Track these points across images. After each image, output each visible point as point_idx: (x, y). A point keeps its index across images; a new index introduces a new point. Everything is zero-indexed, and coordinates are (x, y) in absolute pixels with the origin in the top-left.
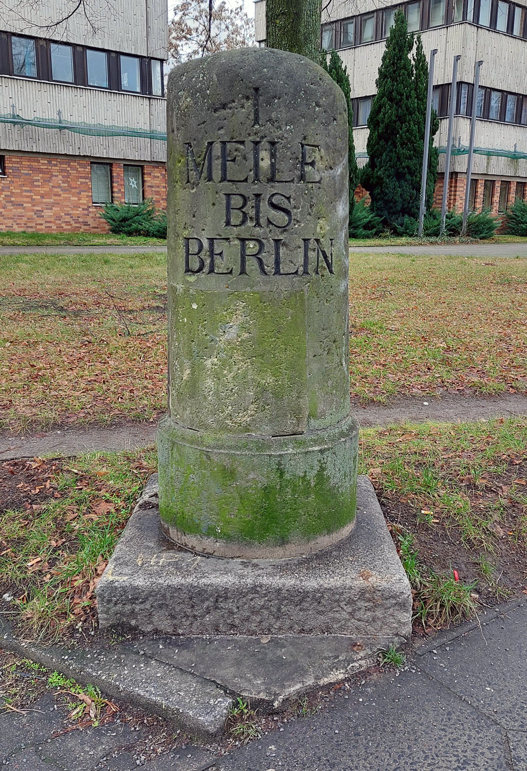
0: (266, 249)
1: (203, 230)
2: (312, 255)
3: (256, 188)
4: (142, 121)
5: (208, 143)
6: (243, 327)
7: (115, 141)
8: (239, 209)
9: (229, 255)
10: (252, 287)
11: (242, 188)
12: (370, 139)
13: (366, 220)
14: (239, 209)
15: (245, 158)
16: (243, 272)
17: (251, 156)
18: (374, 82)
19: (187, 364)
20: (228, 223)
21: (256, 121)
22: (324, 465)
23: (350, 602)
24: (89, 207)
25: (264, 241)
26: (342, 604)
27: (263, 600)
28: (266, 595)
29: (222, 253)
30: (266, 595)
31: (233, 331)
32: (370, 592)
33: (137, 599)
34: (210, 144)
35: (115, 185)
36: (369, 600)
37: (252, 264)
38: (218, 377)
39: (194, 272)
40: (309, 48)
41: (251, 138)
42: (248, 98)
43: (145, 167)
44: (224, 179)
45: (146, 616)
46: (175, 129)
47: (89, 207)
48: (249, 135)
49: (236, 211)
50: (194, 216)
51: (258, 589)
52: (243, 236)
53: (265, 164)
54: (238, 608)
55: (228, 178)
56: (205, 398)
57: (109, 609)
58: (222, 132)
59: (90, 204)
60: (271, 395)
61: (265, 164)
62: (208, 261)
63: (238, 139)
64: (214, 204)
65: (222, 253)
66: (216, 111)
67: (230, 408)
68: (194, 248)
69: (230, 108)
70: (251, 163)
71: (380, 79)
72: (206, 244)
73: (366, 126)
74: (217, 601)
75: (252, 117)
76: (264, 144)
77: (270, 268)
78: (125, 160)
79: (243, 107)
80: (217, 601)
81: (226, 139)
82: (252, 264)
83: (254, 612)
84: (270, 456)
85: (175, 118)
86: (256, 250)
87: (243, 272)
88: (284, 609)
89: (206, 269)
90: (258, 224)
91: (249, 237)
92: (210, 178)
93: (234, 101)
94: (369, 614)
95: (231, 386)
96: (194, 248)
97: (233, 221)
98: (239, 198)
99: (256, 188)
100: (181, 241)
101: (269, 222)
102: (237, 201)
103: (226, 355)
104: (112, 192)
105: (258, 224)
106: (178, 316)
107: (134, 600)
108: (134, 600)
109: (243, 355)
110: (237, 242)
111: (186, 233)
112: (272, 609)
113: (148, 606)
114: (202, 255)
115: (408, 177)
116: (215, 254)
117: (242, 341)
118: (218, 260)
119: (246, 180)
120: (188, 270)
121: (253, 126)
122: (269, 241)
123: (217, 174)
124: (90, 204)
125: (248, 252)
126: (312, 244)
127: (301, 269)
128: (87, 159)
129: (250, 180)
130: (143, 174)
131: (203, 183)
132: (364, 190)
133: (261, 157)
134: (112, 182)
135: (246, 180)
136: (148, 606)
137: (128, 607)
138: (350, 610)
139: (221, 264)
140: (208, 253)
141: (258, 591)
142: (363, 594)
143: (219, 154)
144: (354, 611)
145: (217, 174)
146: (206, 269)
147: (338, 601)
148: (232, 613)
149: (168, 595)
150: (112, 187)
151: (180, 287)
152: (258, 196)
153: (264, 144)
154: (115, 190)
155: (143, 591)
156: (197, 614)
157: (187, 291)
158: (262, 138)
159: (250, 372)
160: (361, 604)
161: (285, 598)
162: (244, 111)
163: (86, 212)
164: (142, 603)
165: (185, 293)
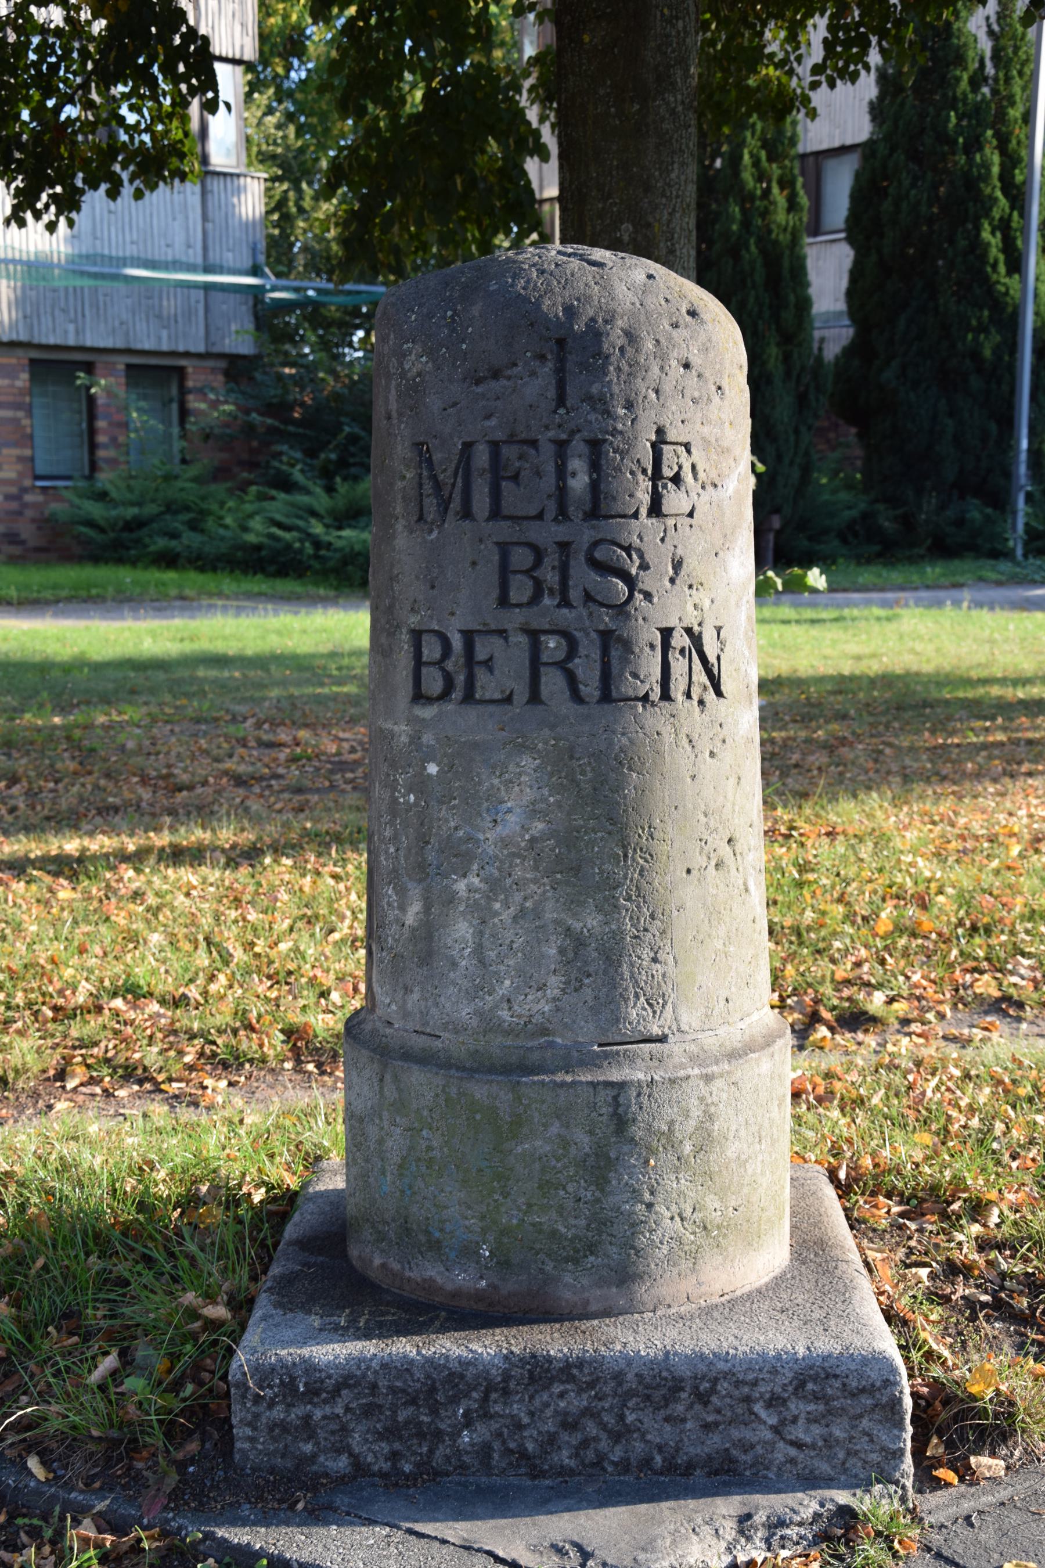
0: (582, 651)
1: (453, 614)
2: (679, 666)
3: (560, 532)
4: (179, 240)
5: (464, 444)
6: (533, 812)
7: (101, 298)
8: (527, 572)
9: (506, 667)
10: (552, 727)
11: (536, 533)
12: (856, 274)
13: (848, 514)
14: (527, 572)
15: (538, 474)
16: (535, 697)
17: (550, 468)
18: (865, 108)
19: (415, 891)
20: (503, 601)
21: (561, 400)
22: (713, 1109)
23: (774, 1402)
24: (24, 490)
25: (578, 634)
26: (758, 1408)
27: (585, 1396)
28: (591, 1385)
29: (491, 659)
30: (591, 1385)
31: (511, 818)
32: (815, 1379)
33: (317, 1393)
34: (468, 446)
35: (101, 424)
36: (816, 1398)
37: (552, 682)
38: (482, 915)
39: (430, 700)
40: (668, 104)
41: (551, 434)
42: (542, 358)
43: (190, 370)
44: (496, 513)
45: (333, 1433)
46: (394, 414)
47: (24, 490)
48: (547, 427)
49: (519, 576)
50: (433, 587)
51: (575, 1371)
52: (535, 625)
53: (579, 482)
54: (532, 1414)
55: (505, 512)
56: (454, 964)
57: (257, 1416)
58: (493, 422)
59: (27, 482)
60: (595, 954)
61: (579, 482)
62: (460, 679)
63: (523, 436)
64: (474, 564)
65: (491, 659)
66: (478, 382)
67: (507, 983)
68: (431, 650)
69: (509, 378)
70: (549, 481)
71: (881, 97)
72: (457, 643)
73: (842, 235)
74: (485, 1399)
75: (552, 393)
76: (578, 445)
77: (591, 689)
78: (129, 351)
79: (533, 374)
80: (485, 1399)
81: (499, 435)
82: (552, 682)
83: (569, 1423)
84: (594, 1085)
85: (393, 392)
86: (561, 655)
87: (535, 697)
88: (630, 1418)
89: (457, 695)
90: (565, 602)
91: (547, 627)
92: (467, 513)
93: (515, 365)
94: (817, 1430)
95: (509, 935)
96: (431, 650)
97: (514, 597)
98: (527, 551)
99: (560, 532)
100: (405, 637)
101: (588, 597)
102: (521, 558)
103: (499, 869)
104: (93, 446)
105: (565, 602)
106: (395, 789)
107: (313, 1392)
108: (313, 1392)
109: (536, 868)
110: (523, 639)
111: (413, 620)
112: (606, 1418)
113: (339, 1410)
114: (449, 665)
115: (976, 382)
116: (480, 663)
117: (533, 840)
118: (481, 676)
119: (540, 516)
120: (419, 697)
121: (555, 412)
122: (588, 634)
123: (481, 502)
124: (27, 482)
125: (545, 658)
126: (680, 640)
127: (657, 689)
128: (20, 352)
129: (549, 515)
130: (183, 391)
131: (451, 523)
132: (841, 422)
133: (570, 468)
134: (92, 417)
135: (540, 516)
136: (339, 1410)
137: (300, 1410)
138: (773, 1421)
139: (487, 685)
140: (462, 660)
141: (574, 1377)
142: (802, 1384)
143: (487, 466)
144: (783, 1422)
145: (481, 502)
146: (457, 695)
147: (748, 1400)
148: (519, 1427)
149: (383, 1383)
150: (92, 431)
151: (402, 731)
152: (564, 546)
153: (578, 445)
154: (101, 439)
155: (330, 1377)
156: (443, 1426)
157: (415, 739)
158: (572, 433)
159: (550, 905)
160: (795, 1407)
161: (631, 1394)
162: (536, 386)
163: (14, 505)
164: (325, 1402)
165: (411, 743)
